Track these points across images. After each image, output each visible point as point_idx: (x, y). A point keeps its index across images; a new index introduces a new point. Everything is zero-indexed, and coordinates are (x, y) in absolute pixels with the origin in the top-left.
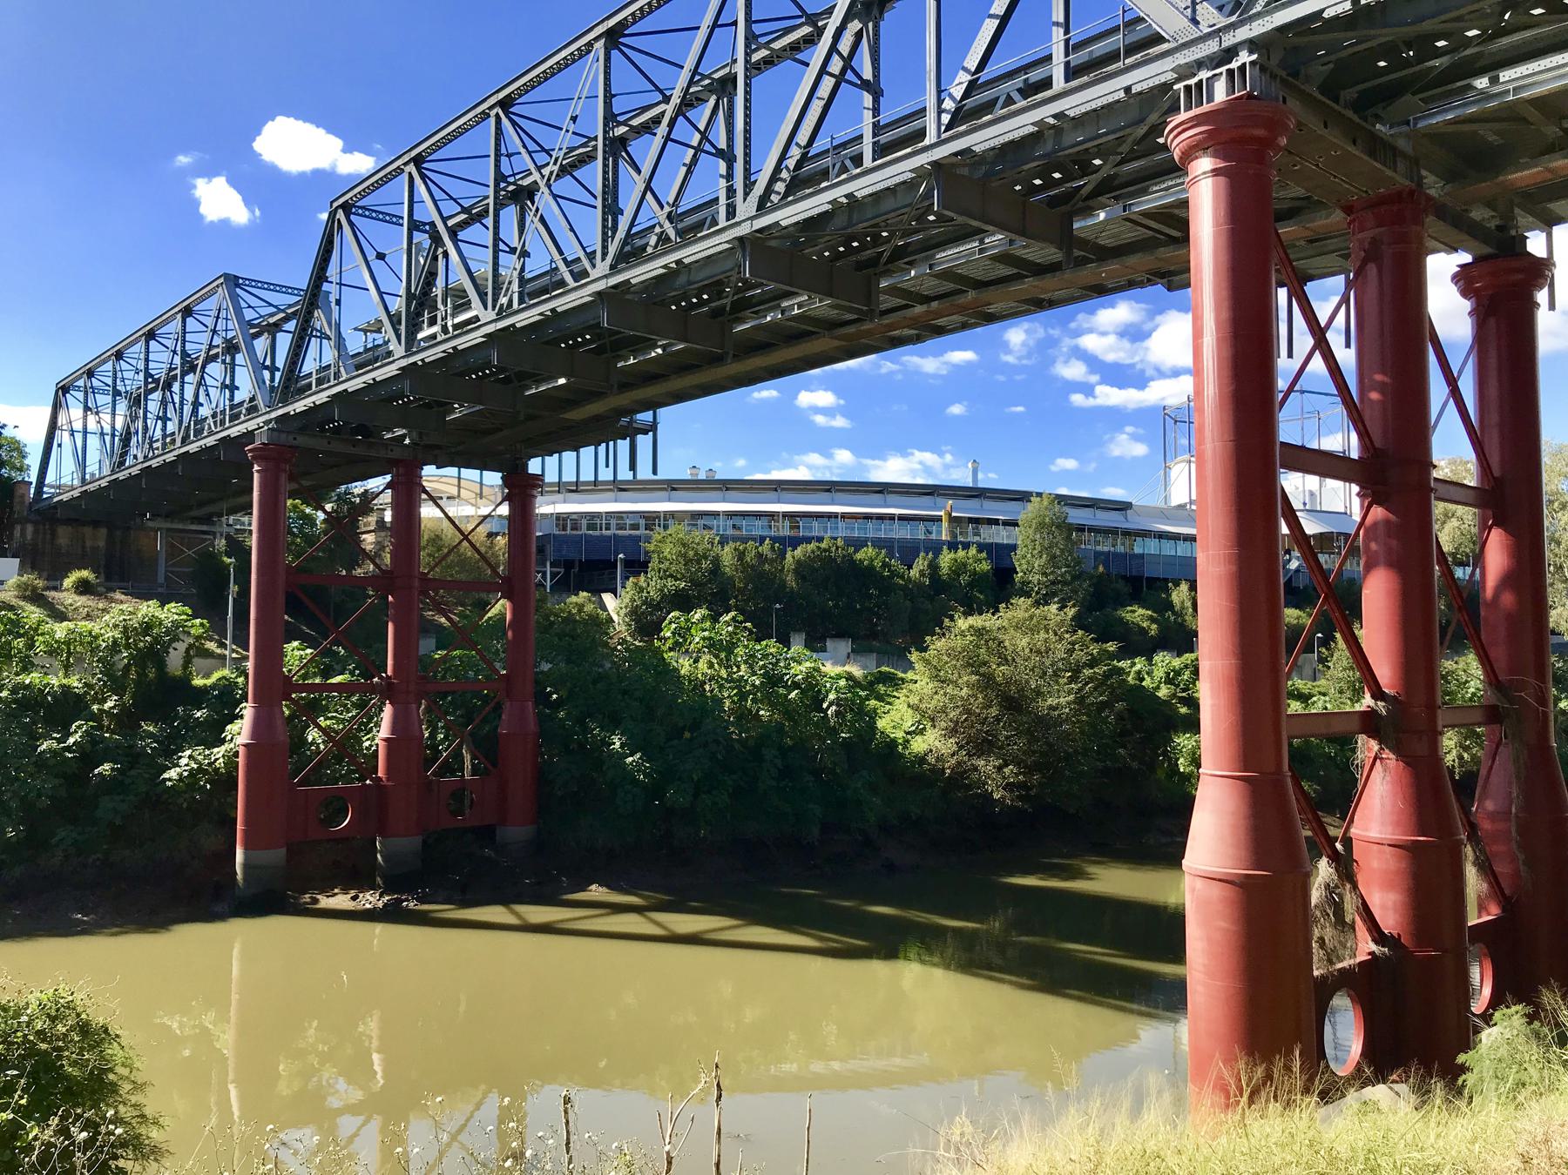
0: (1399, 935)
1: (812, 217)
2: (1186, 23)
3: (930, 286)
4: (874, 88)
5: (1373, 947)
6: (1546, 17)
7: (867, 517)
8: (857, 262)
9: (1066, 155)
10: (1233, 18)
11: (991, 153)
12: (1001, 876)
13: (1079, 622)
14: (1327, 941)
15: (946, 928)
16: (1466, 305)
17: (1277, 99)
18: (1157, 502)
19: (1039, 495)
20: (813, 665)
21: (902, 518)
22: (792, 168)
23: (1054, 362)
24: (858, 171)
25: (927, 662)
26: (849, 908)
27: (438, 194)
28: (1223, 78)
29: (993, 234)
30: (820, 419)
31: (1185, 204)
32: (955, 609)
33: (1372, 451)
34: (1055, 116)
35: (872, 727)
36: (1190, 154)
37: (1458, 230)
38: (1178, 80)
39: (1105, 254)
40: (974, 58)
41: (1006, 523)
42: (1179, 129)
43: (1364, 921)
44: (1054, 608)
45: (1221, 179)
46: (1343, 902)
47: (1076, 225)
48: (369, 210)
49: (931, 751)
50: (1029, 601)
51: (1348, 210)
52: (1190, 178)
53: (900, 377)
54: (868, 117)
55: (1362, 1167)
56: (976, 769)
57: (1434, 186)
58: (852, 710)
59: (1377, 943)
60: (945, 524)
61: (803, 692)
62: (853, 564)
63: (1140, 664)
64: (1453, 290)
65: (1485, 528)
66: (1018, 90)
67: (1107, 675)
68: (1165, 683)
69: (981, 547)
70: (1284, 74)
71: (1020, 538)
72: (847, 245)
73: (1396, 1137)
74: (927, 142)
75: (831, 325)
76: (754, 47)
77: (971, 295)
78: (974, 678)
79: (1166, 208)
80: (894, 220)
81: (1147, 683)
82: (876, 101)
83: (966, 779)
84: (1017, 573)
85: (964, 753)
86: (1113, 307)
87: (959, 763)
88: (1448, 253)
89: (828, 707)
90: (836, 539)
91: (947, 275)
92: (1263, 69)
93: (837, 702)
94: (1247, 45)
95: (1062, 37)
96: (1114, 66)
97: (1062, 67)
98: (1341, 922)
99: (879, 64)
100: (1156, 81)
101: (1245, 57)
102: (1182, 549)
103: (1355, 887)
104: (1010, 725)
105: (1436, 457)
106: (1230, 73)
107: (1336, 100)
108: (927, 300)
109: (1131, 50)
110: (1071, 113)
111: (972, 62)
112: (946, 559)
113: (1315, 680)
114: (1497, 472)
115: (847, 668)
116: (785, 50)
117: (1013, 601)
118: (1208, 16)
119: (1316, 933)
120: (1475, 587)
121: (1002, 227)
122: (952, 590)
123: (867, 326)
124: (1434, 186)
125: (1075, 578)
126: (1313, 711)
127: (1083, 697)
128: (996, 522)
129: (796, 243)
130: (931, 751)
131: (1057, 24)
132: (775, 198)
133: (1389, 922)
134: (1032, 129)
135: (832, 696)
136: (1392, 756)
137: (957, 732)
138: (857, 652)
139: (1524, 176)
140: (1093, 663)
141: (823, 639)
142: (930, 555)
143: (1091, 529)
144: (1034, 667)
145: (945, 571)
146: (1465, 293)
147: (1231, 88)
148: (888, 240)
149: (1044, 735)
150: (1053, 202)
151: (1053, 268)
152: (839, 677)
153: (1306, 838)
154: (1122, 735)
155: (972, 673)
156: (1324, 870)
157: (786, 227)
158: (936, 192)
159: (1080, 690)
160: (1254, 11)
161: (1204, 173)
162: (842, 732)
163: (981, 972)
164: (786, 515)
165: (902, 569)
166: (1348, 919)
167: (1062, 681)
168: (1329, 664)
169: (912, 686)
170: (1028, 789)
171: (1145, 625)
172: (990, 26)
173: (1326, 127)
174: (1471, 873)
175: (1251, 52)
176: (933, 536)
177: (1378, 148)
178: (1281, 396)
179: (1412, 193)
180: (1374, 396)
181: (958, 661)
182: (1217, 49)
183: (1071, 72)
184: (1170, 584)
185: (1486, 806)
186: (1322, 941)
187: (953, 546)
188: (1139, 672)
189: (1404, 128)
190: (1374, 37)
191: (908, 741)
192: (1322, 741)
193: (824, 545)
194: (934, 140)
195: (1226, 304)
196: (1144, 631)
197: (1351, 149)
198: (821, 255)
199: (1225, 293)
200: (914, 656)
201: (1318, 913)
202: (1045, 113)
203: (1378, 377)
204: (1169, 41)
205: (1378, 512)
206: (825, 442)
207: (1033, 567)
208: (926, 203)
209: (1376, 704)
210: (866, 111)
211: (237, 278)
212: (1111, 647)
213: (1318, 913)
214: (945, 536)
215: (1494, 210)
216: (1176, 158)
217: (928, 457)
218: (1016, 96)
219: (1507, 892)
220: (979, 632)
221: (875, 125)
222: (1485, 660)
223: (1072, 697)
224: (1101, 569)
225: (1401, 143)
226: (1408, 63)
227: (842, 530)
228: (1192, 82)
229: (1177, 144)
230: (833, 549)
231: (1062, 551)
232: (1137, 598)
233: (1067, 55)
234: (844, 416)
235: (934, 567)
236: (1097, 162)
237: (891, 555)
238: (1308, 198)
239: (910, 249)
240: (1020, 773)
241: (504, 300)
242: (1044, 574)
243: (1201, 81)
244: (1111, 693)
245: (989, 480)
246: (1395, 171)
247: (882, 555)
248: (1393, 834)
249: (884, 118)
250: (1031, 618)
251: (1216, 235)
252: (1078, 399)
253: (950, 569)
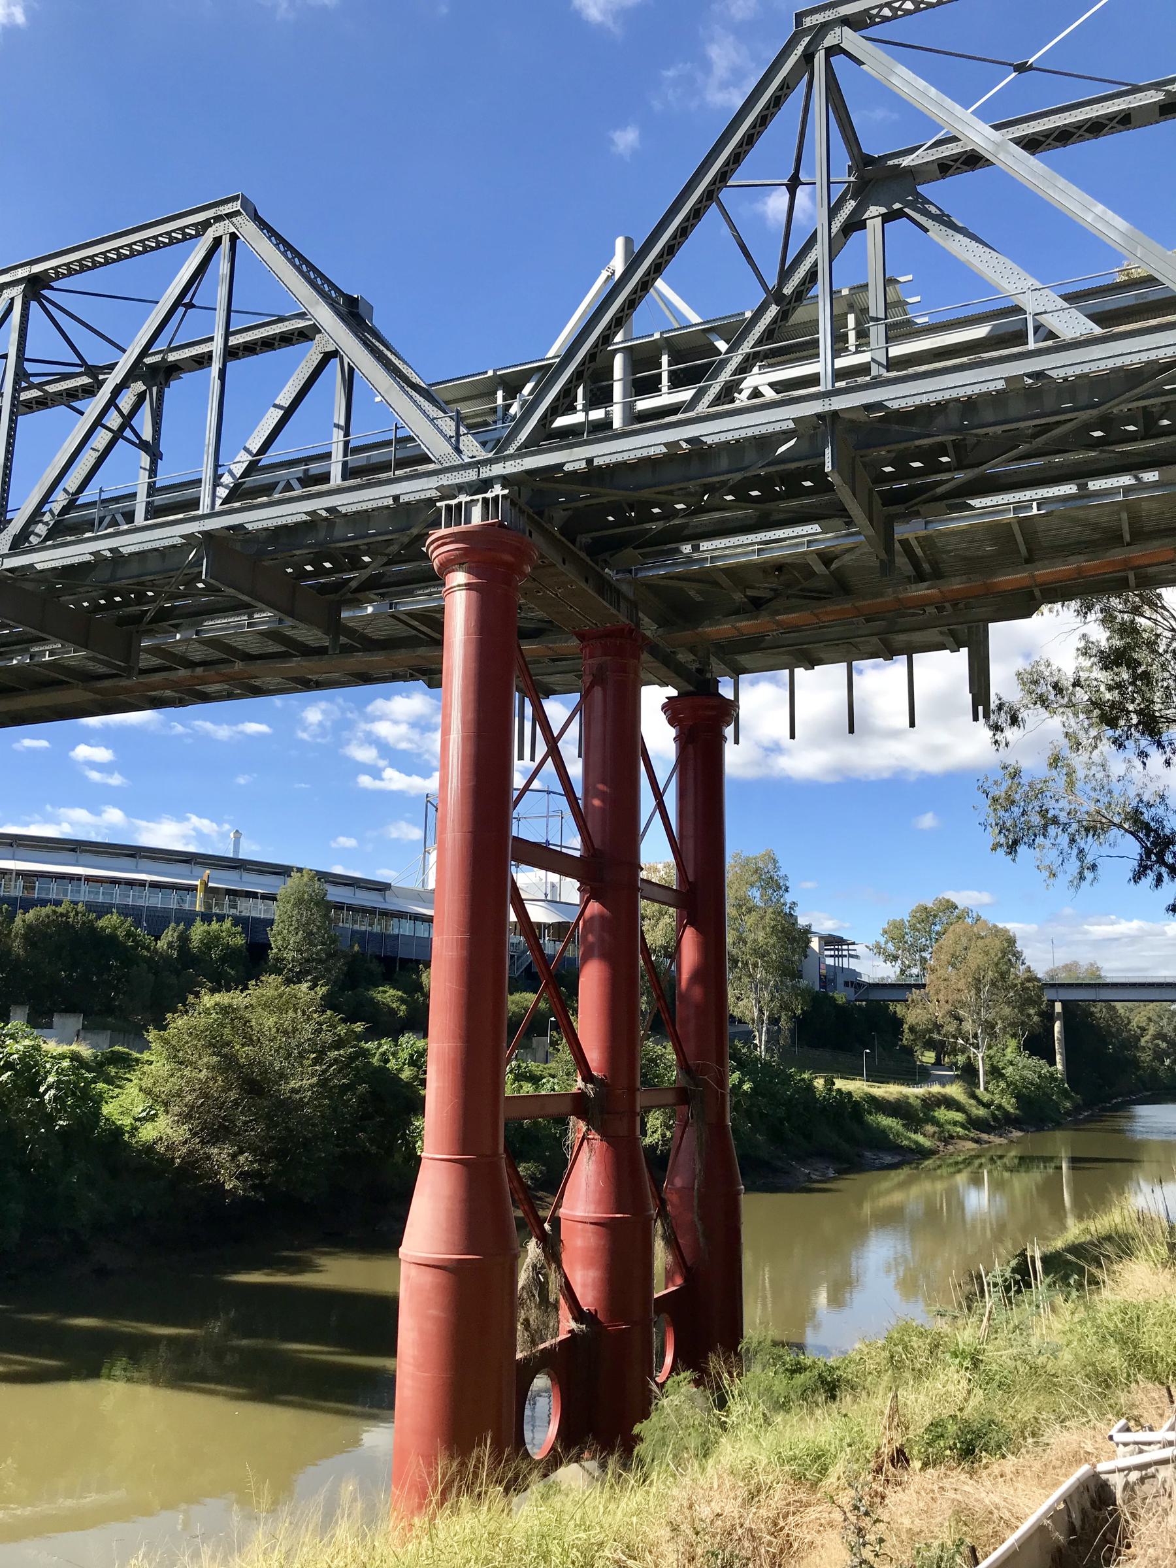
0: (596, 1311)
1: (72, 566)
2: (450, 450)
3: (198, 653)
4: (153, 450)
5: (573, 1325)
6: (735, 504)
7: (115, 881)
8: (119, 617)
9: (336, 548)
10: (490, 455)
11: (264, 533)
12: (225, 1274)
13: (328, 1002)
14: (531, 1322)
15: (157, 1339)
16: (672, 732)
17: (524, 532)
18: (414, 884)
19: (300, 870)
20: (33, 1043)
21: (154, 885)
22: (56, 512)
23: (348, 742)
24: (126, 527)
25: (166, 1042)
26: (43, 1322)
28: (480, 504)
29: (262, 611)
30: (95, 776)
31: (441, 610)
32: (201, 985)
33: (592, 851)
34: (327, 510)
35: (96, 1114)
36: (448, 566)
37: (670, 669)
38: (442, 499)
39: (371, 645)
40: (256, 441)
41: (265, 897)
42: (439, 542)
43: (566, 1300)
44: (304, 986)
45: (473, 593)
46: (548, 1282)
47: (344, 615)
49: (161, 1139)
50: (280, 979)
51: (582, 637)
52: (447, 587)
53: (189, 741)
54: (144, 477)
55: (535, 1555)
56: (209, 1158)
57: (649, 628)
58: (74, 1094)
59: (576, 1320)
60: (200, 894)
61: (17, 1074)
62: (91, 928)
63: (386, 1045)
64: (663, 718)
65: (681, 928)
66: (297, 479)
67: (352, 1058)
68: (409, 1065)
69: (237, 921)
70: (531, 511)
71: (278, 913)
72: (109, 597)
73: (567, 1518)
74: (200, 512)
75: (86, 677)
76: (24, 385)
77: (238, 666)
78: (215, 1059)
79: (429, 611)
80: (160, 582)
81: (392, 1064)
82: (154, 463)
83: (197, 1168)
84: (272, 949)
85: (198, 1140)
86: (408, 697)
87: (191, 1152)
88: (661, 685)
89: (46, 1091)
90: (76, 903)
91: (214, 643)
92: (513, 503)
93: (57, 1085)
94: (500, 481)
95: (341, 438)
96: (385, 475)
97: (340, 466)
98: (547, 1306)
99: (160, 428)
100: (423, 496)
101: (498, 490)
102: (421, 930)
103: (559, 1266)
104: (250, 1109)
105: (644, 861)
106: (485, 501)
107: (573, 542)
108: (192, 665)
109: (401, 464)
110: (343, 510)
111: (255, 445)
112: (198, 931)
113: (547, 1062)
114: (691, 879)
115: (74, 1047)
116: (62, 395)
117: (263, 978)
118: (473, 448)
119: (522, 1315)
120: (674, 982)
121: (272, 605)
122: (202, 965)
123: (124, 683)
124: (649, 628)
125: (330, 956)
126: (543, 1093)
127: (326, 1079)
128: (254, 895)
129: (51, 589)
130: (161, 1139)
131: (338, 426)
132: (34, 540)
133: (587, 1298)
134: (305, 518)
135: (51, 1079)
136: (597, 1137)
137: (191, 1117)
138: (88, 1029)
139: (722, 629)
140: (338, 1044)
141: (50, 1014)
142: (182, 926)
143: (352, 908)
144: (280, 1047)
145: (195, 944)
146: (671, 722)
147: (485, 516)
148: (152, 600)
149: (283, 1120)
150: (323, 589)
151: (321, 651)
152: (63, 1057)
153: (516, 1218)
154: (362, 1118)
155: (214, 1054)
156: (533, 1250)
157: (42, 571)
158: (205, 561)
159: (324, 1072)
160: (507, 452)
161: (459, 586)
162: (60, 1119)
163: (193, 1384)
164: (20, 874)
165: (148, 939)
166: (552, 1299)
167: (307, 1062)
168: (559, 1047)
169: (146, 1067)
170: (265, 1177)
172: (275, 415)
173: (564, 563)
174: (659, 1246)
175: (504, 487)
176: (187, 907)
177: (604, 587)
178: (516, 794)
179: (631, 631)
180: (597, 802)
181: (199, 1040)
182: (475, 478)
183: (348, 472)
184: (421, 966)
185: (677, 1181)
186: (526, 1322)
187: (207, 918)
188: (384, 1054)
189: (628, 575)
190: (605, 495)
191: (136, 1129)
192: (549, 1122)
193: (60, 910)
194: (207, 511)
195: (471, 706)
196: (393, 1012)
197: (583, 585)
198: (78, 603)
199: (471, 696)
200: (152, 1035)
201: (525, 1295)
202: (319, 505)
203: (600, 786)
204: (434, 462)
205: (594, 907)
206: (95, 799)
207: (289, 944)
208: (196, 570)
209: (586, 1087)
210: (142, 471)
212: (359, 1027)
213: (525, 1295)
214: (199, 907)
215: (695, 655)
216: (435, 567)
217: (206, 825)
218: (295, 483)
219: (689, 1264)
220: (225, 1010)
221: (151, 486)
222: (679, 1050)
223: (315, 1080)
224: (356, 948)
225: (624, 588)
226: (630, 522)
227: (85, 894)
228: (453, 502)
229: (438, 555)
230: (72, 915)
231: (319, 928)
232: (388, 978)
233: (345, 455)
234: (121, 773)
235: (184, 939)
236: (366, 559)
237: (137, 923)
238: (551, 622)
239: (177, 612)
240: (256, 1161)
242: (300, 951)
243: (460, 503)
244: (355, 1076)
245: (250, 851)
246: (619, 611)
247: (127, 924)
248: (595, 1213)
249: (162, 480)
250: (281, 996)
251: (467, 642)
252: (365, 781)
253: (202, 942)
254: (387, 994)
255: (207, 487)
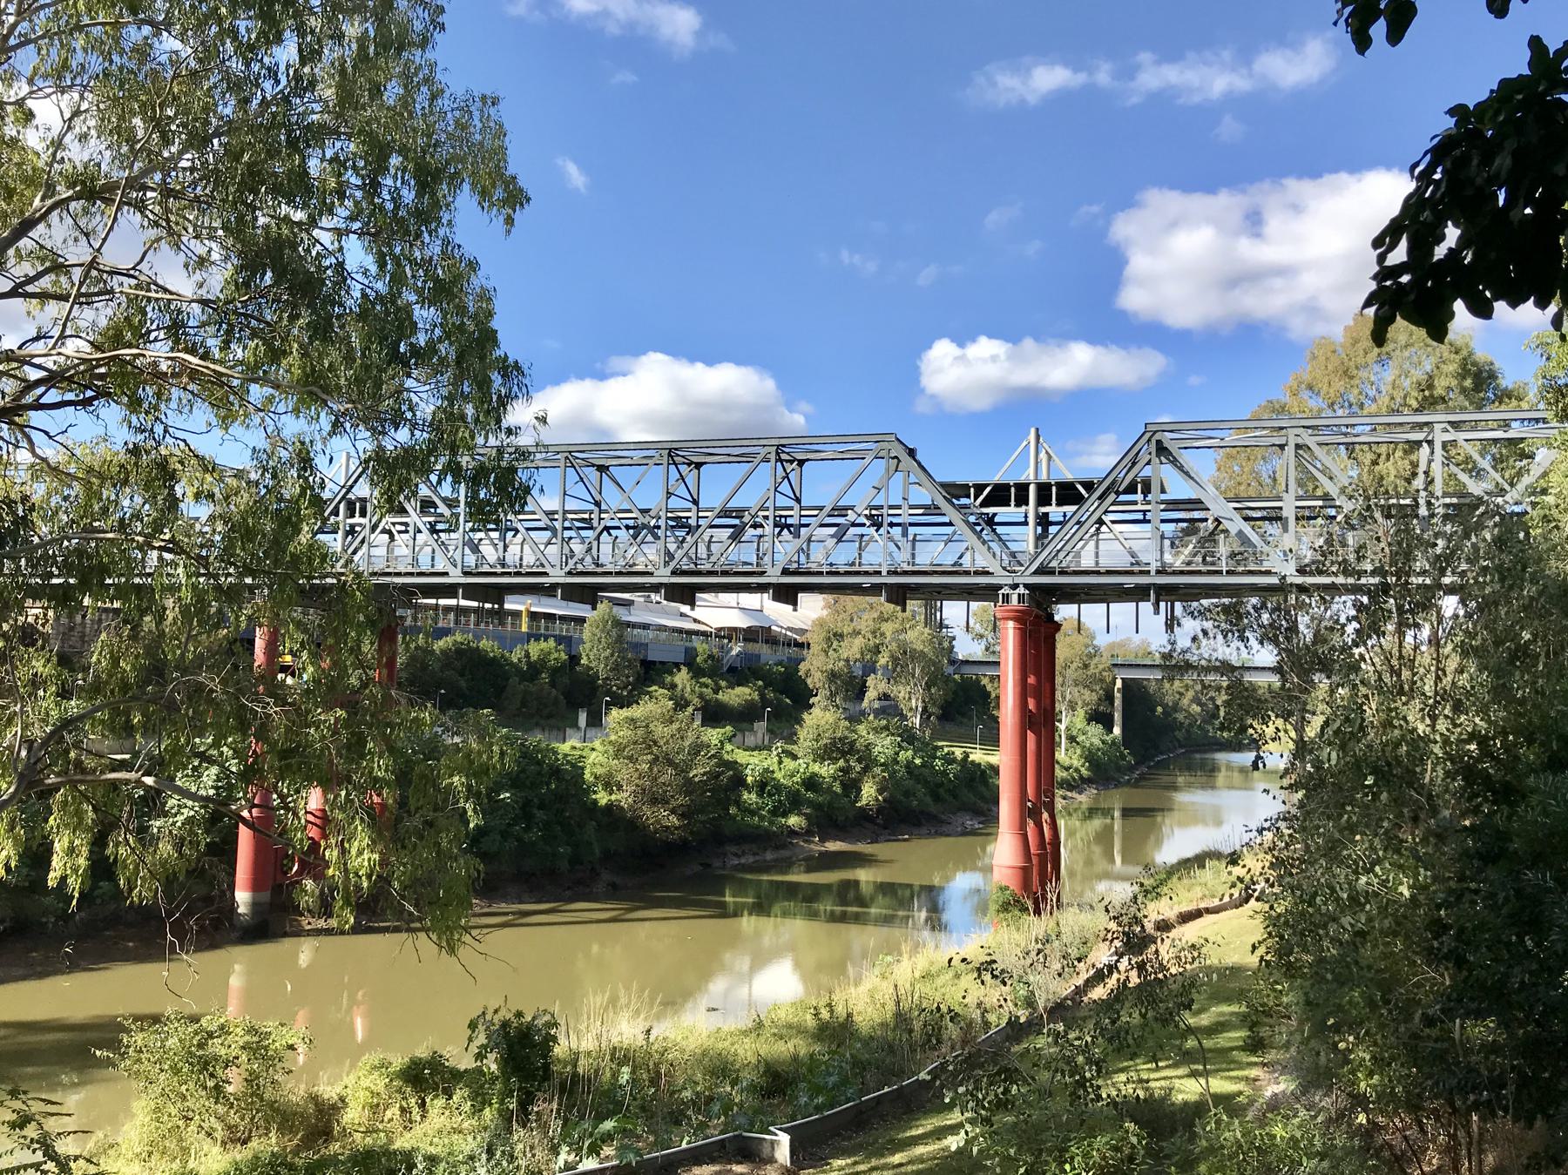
60: (525, 619)
101: (1021, 590)
112: (535, 649)
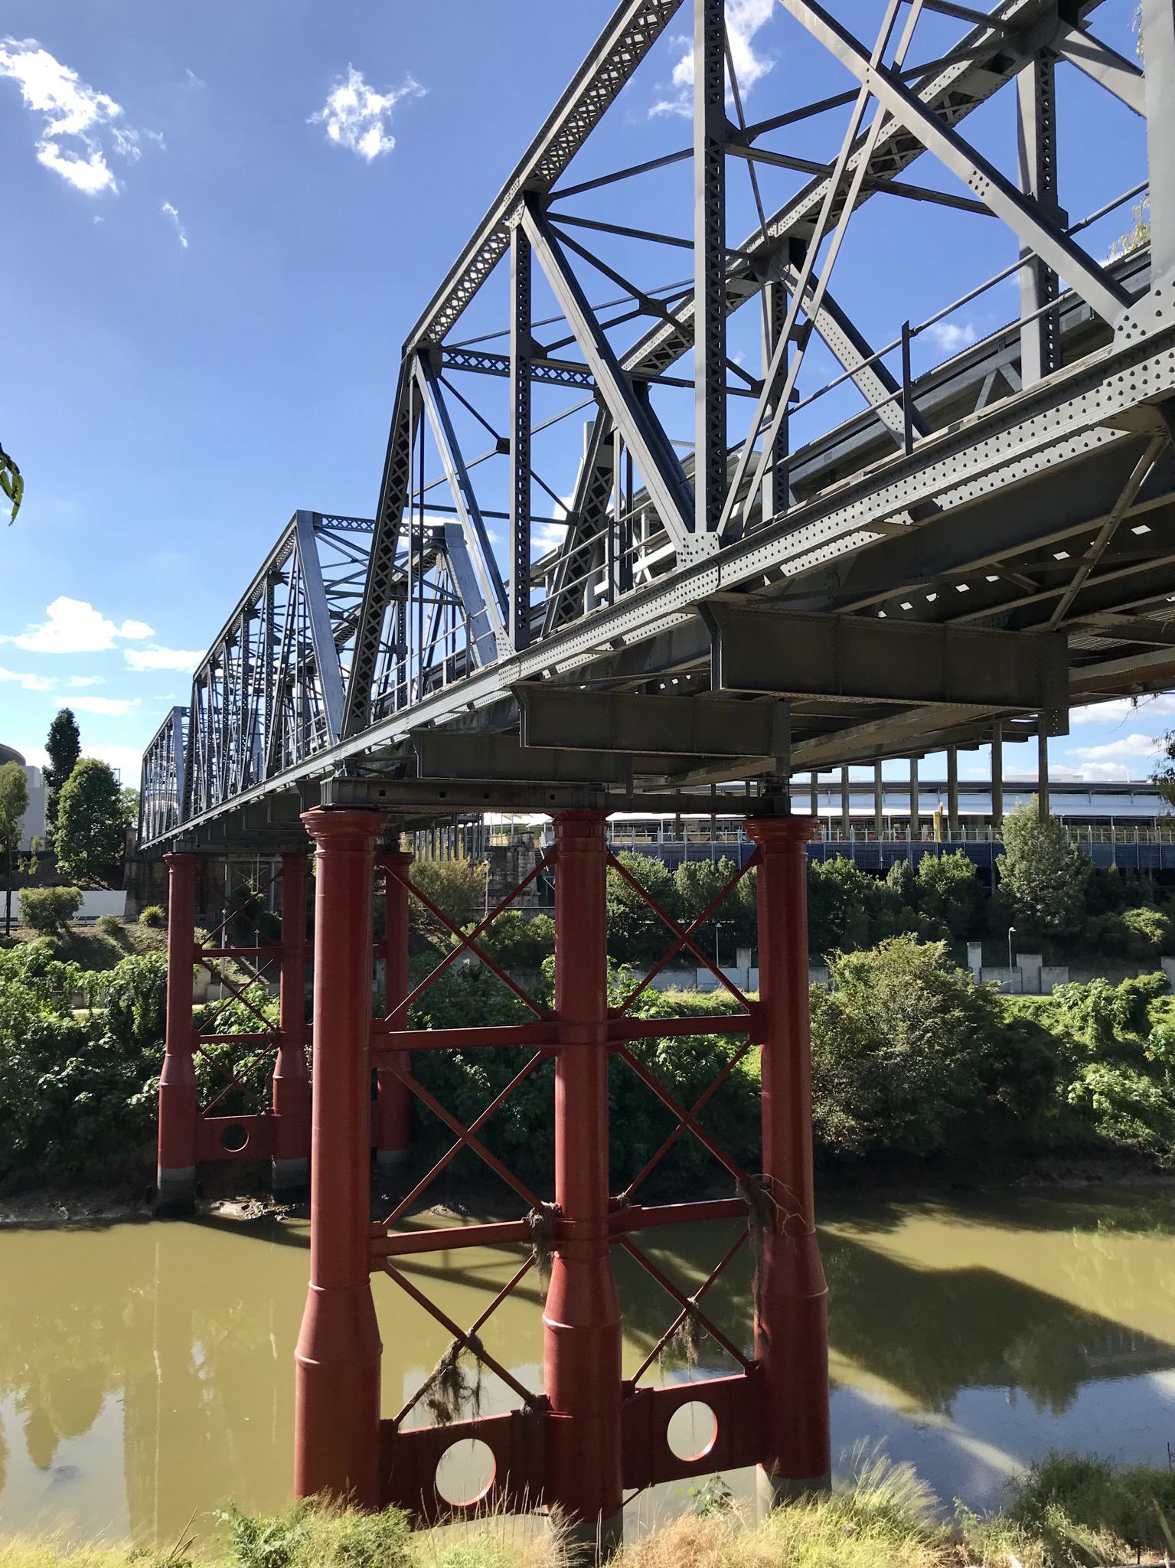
27: (598, 289)
48: (463, 353)
112: (926, 864)
171: (1147, 930)
196: (1145, 937)
211: (317, 517)
235: (912, 873)
241: (730, 510)
254: (1143, 917)
255: (694, 586)
